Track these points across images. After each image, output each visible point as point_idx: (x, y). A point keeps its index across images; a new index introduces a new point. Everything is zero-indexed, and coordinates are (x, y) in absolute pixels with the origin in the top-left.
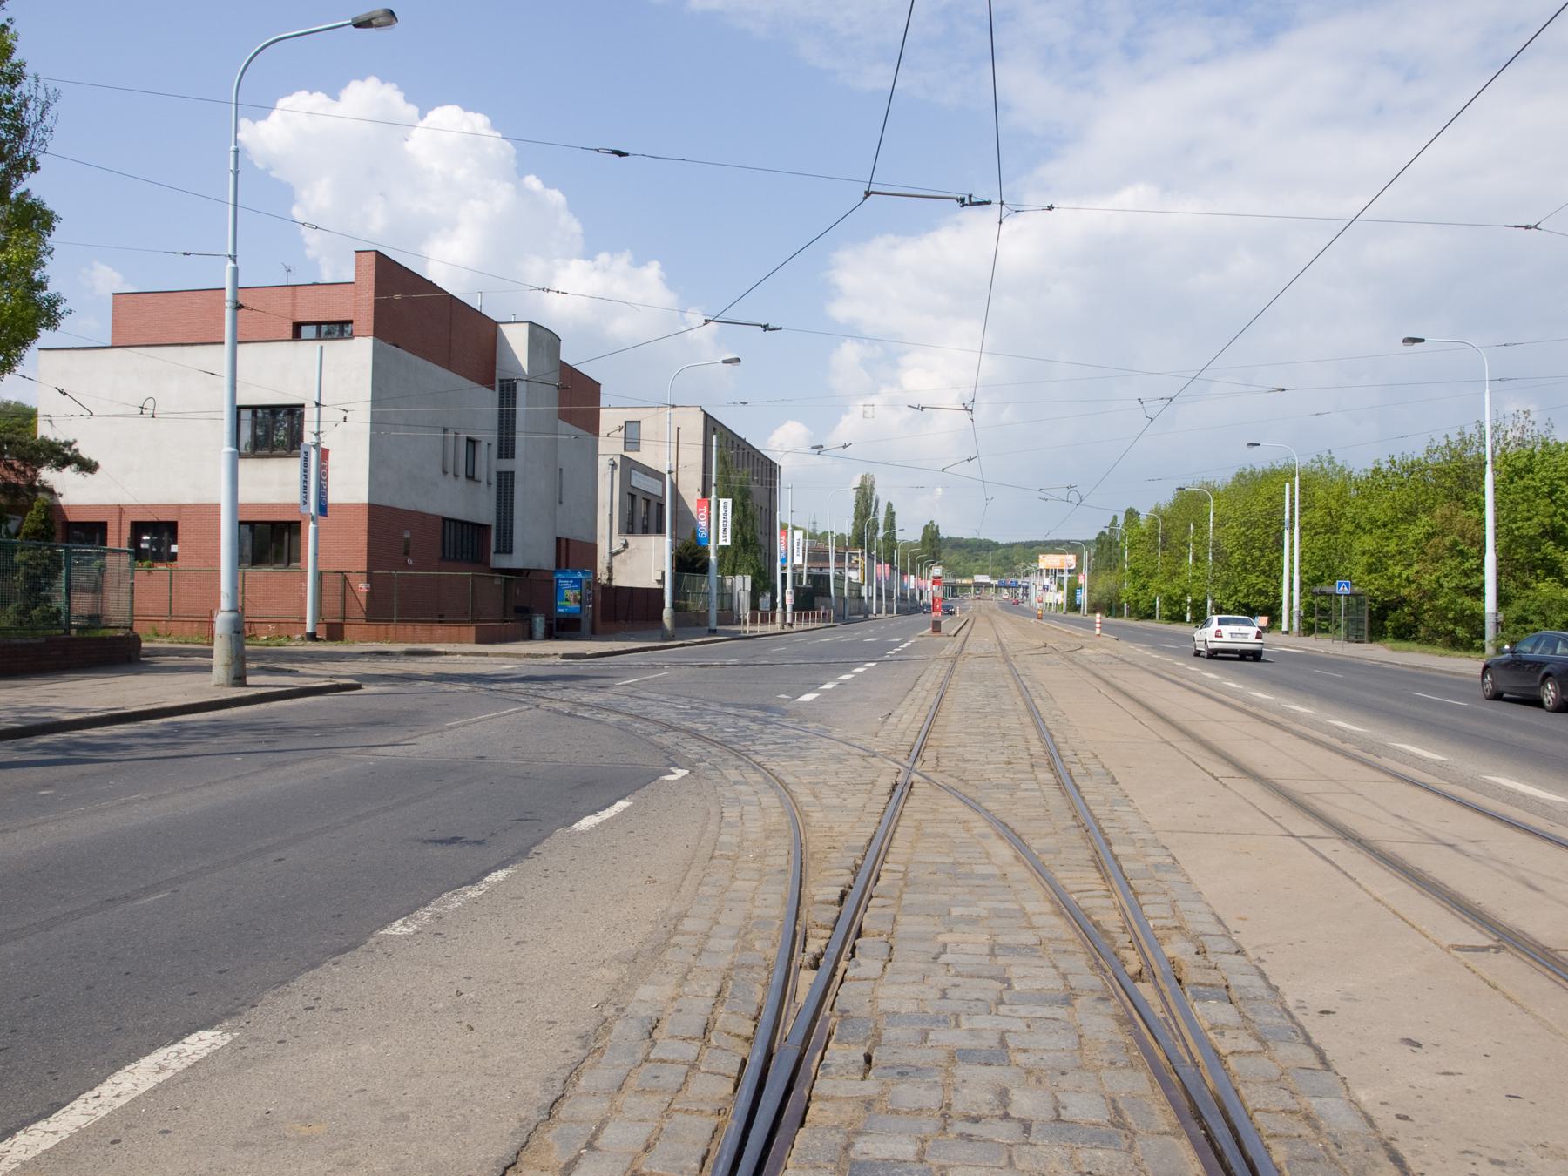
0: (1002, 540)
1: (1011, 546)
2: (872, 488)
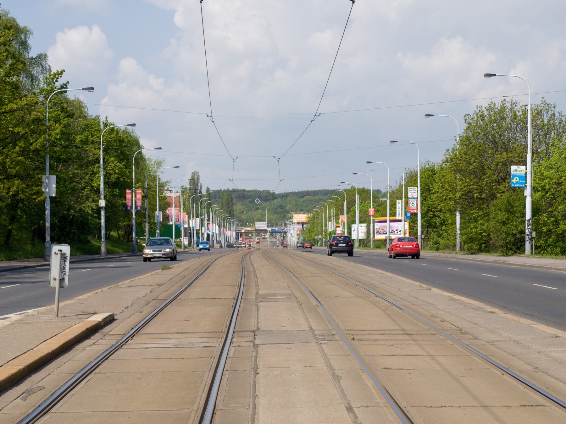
0: (279, 190)
1: (285, 196)
2: (198, 179)
